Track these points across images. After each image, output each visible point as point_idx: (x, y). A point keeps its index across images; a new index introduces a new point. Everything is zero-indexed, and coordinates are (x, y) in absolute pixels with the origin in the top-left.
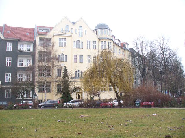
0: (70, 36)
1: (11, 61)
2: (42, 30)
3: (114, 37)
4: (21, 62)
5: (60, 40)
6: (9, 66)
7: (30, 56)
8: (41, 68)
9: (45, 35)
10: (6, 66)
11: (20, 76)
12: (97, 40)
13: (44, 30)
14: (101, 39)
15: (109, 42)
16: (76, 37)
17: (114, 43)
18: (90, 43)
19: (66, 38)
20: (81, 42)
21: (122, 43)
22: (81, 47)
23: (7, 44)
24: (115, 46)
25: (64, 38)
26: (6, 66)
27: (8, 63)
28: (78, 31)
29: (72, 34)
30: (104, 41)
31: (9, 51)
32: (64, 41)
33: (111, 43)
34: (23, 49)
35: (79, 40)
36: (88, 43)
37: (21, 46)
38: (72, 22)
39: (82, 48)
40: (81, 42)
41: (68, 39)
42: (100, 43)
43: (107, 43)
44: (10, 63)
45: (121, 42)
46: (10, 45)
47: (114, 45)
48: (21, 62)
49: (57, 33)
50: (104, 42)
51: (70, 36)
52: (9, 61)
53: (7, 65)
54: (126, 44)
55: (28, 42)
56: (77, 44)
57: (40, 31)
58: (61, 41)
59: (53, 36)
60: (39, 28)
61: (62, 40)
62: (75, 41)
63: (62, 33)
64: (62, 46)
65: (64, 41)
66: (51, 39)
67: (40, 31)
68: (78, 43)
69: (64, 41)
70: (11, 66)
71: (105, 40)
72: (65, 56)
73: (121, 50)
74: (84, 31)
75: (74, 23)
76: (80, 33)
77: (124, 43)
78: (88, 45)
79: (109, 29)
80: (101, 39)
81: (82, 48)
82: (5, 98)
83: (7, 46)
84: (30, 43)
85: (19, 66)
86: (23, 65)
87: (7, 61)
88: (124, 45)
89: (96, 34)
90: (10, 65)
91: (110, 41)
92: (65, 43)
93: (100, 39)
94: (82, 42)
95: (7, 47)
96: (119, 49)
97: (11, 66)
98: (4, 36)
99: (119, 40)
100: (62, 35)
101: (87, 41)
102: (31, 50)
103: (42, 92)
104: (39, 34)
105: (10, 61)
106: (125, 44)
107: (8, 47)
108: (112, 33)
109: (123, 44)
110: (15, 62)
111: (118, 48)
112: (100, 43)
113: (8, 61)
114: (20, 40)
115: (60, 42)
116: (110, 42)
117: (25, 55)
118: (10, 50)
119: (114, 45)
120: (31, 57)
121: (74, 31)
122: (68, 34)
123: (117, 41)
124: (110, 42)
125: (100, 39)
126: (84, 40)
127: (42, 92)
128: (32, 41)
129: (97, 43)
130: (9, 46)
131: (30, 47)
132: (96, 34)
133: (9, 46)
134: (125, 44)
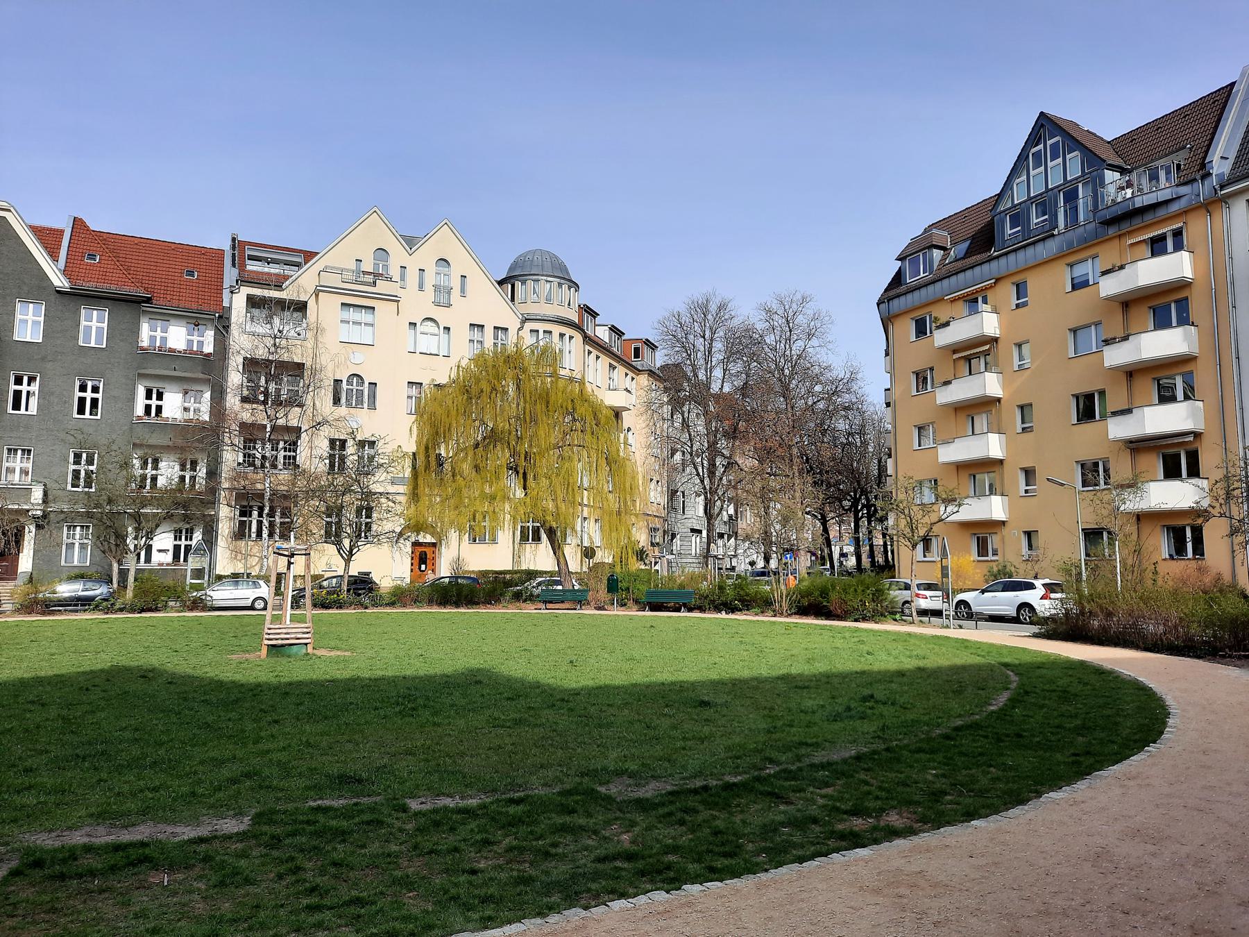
0: (394, 299)
3: (594, 314)
4: (154, 402)
8: (250, 433)
9: (279, 287)
23: (83, 311)
28: (430, 279)
29: (400, 293)
31: (93, 344)
33: (571, 338)
34: (164, 339)
37: (153, 329)
46: (100, 320)
47: (587, 347)
48: (154, 402)
49: (333, 280)
51: (394, 299)
59: (317, 293)
72: (366, 384)
74: (456, 283)
79: (571, 281)
82: (63, 563)
83: (83, 323)
86: (165, 414)
87: (13, 387)
88: (637, 350)
89: (513, 299)
91: (568, 331)
95: (82, 328)
96: (612, 367)
98: (65, 272)
99: (613, 329)
102: (209, 348)
103: (366, 405)
107: (89, 328)
111: (605, 361)
116: (567, 336)
118: (99, 340)
121: (412, 277)
122: (382, 287)
123: (603, 334)
124: (567, 336)
127: (366, 405)
130: (94, 324)
132: (513, 299)
133: (94, 324)
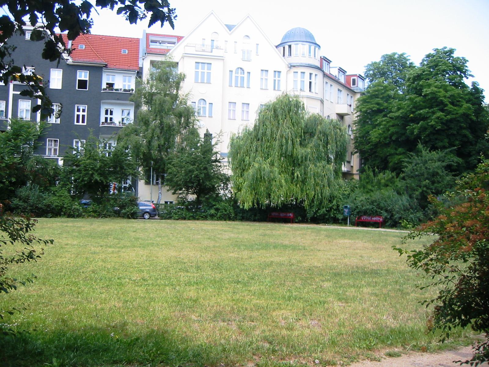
0: (221, 58)
1: (85, 114)
2: (158, 44)
3: (329, 62)
4: (109, 116)
5: (197, 68)
6: (81, 123)
7: (128, 102)
10: (76, 123)
11: (107, 113)
12: (283, 68)
13: (163, 42)
14: (294, 66)
15: (311, 74)
16: (234, 62)
17: (325, 75)
18: (279, 77)
19: (211, 64)
20: (246, 74)
21: (347, 76)
22: (245, 85)
24: (327, 83)
25: (208, 64)
26: (76, 123)
27: (78, 116)
30: (300, 70)
32: (208, 70)
33: (316, 75)
35: (241, 69)
36: (275, 76)
38: (227, 25)
39: (248, 87)
40: (246, 74)
41: (216, 66)
42: (291, 74)
43: (307, 75)
44: (83, 116)
45: (347, 74)
48: (109, 116)
49: (191, 51)
50: (299, 74)
51: (221, 58)
52: (81, 113)
53: (78, 121)
54: (359, 79)
55: (124, 70)
56: (237, 77)
57: (153, 46)
58: (200, 70)
59: (183, 57)
60: (151, 38)
61: (203, 68)
62: (231, 71)
63: (203, 51)
64: (202, 82)
65: (206, 71)
66: (178, 63)
67: (153, 46)
68: (239, 75)
69: (208, 70)
70: (85, 124)
71: (303, 69)
73: (344, 92)
75: (230, 28)
76: (244, 52)
77: (355, 75)
78: (275, 80)
79: (316, 44)
80: (294, 66)
81: (248, 87)
84: (129, 73)
85: (104, 89)
87: (76, 113)
90: (83, 122)
91: (314, 72)
92: (209, 74)
93: (291, 66)
94: (249, 73)
97: (85, 124)
99: (341, 70)
100: (201, 57)
101: (273, 72)
104: (150, 52)
105: (84, 113)
106: (356, 78)
108: (322, 53)
109: (352, 78)
110: (94, 114)
111: (336, 87)
112: (291, 74)
113: (78, 113)
114: (106, 65)
115: (197, 73)
117: (118, 99)
119: (326, 80)
120: (131, 105)
122: (216, 52)
123: (334, 72)
125: (291, 66)
126: (254, 68)
128: (134, 68)
129: (283, 75)
131: (129, 82)
134: (356, 78)
